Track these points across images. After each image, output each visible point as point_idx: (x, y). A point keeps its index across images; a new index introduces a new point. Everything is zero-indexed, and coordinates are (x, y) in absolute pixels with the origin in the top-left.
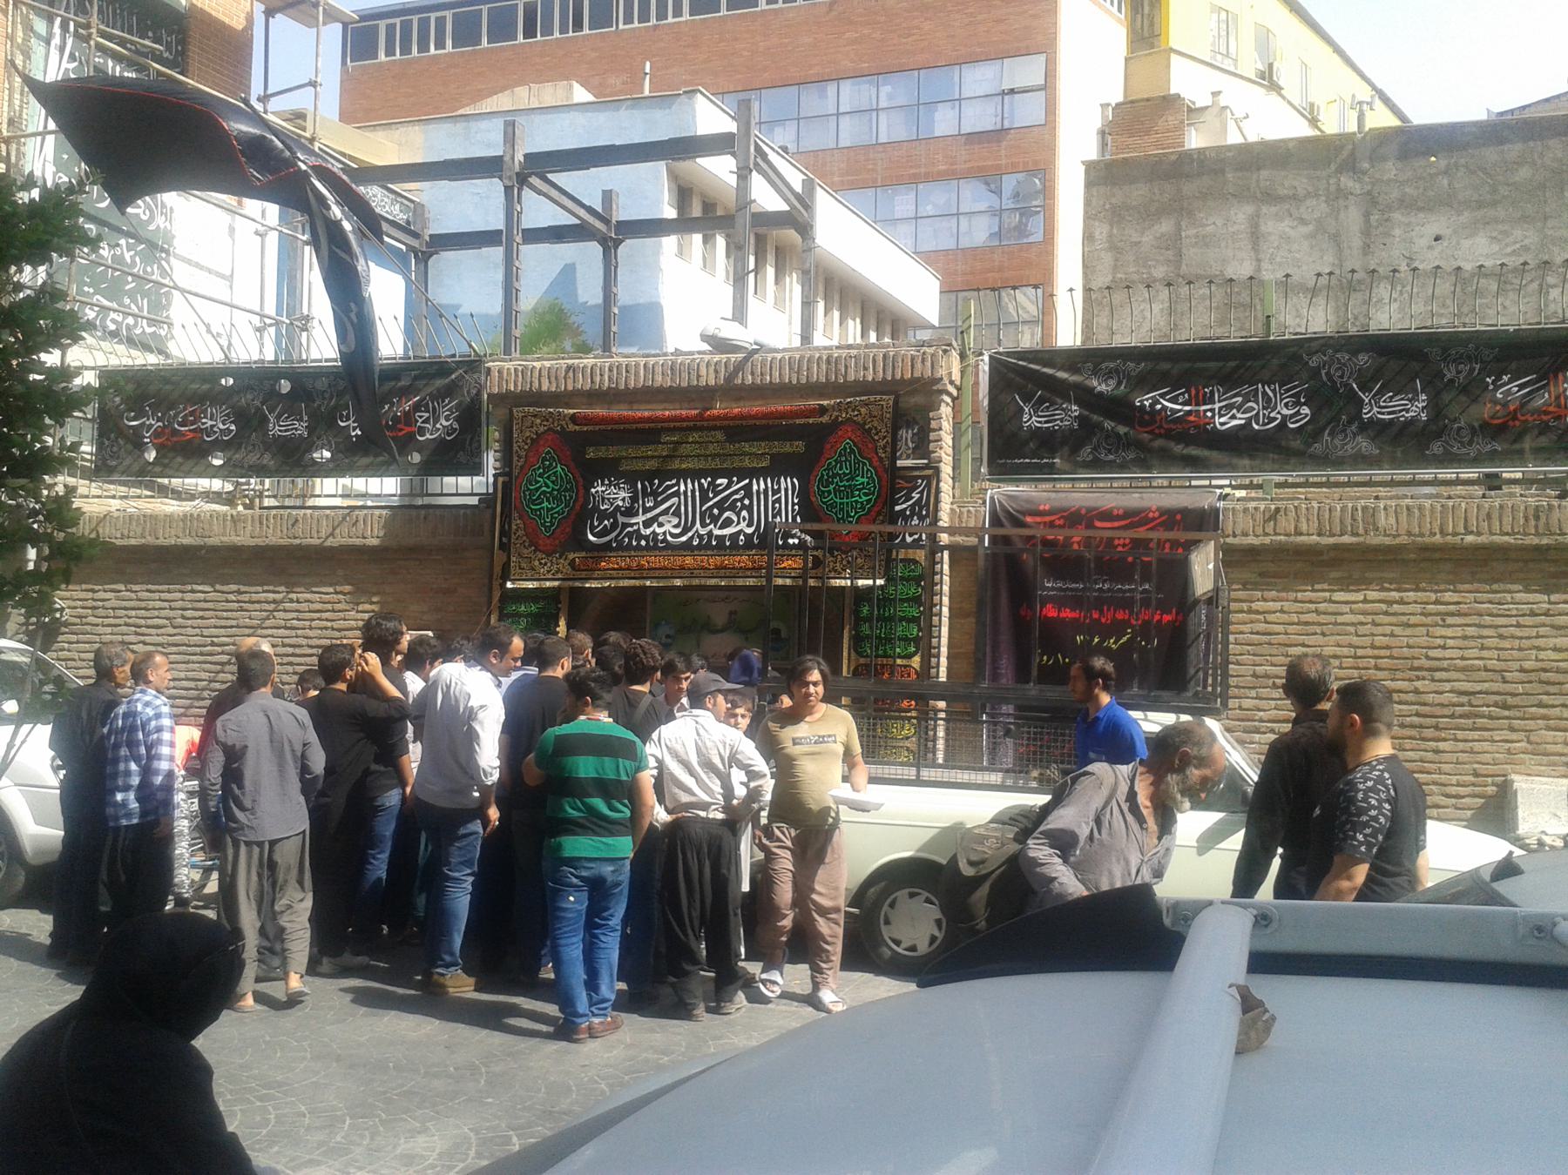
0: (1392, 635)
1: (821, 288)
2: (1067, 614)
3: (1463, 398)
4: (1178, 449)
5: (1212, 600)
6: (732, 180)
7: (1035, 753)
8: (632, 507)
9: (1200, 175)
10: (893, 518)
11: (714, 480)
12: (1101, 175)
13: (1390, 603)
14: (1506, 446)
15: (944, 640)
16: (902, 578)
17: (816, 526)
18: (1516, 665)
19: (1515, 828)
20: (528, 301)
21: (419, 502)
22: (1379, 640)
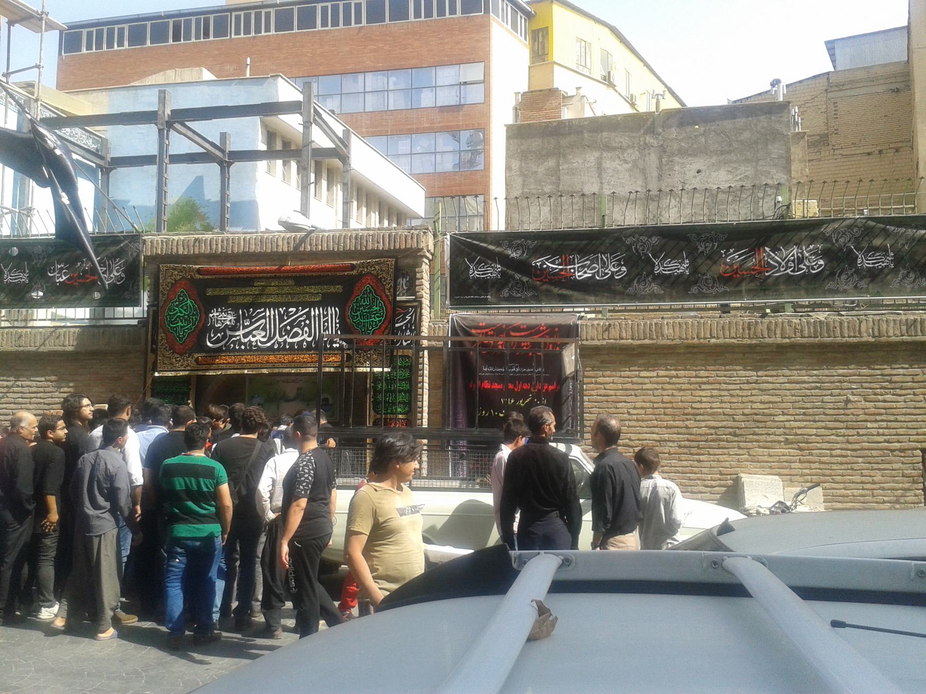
0: (673, 395)
1: (355, 194)
2: (496, 386)
3: (709, 262)
4: (556, 290)
5: (575, 377)
6: (300, 129)
7: (478, 468)
8: (236, 325)
9: (570, 134)
10: (394, 331)
11: (287, 308)
12: (516, 133)
13: (671, 377)
14: (732, 289)
15: (426, 403)
16: (400, 367)
17: (348, 336)
18: (740, 412)
19: (744, 504)
20: (173, 197)
21: (102, 323)
22: (666, 398)
